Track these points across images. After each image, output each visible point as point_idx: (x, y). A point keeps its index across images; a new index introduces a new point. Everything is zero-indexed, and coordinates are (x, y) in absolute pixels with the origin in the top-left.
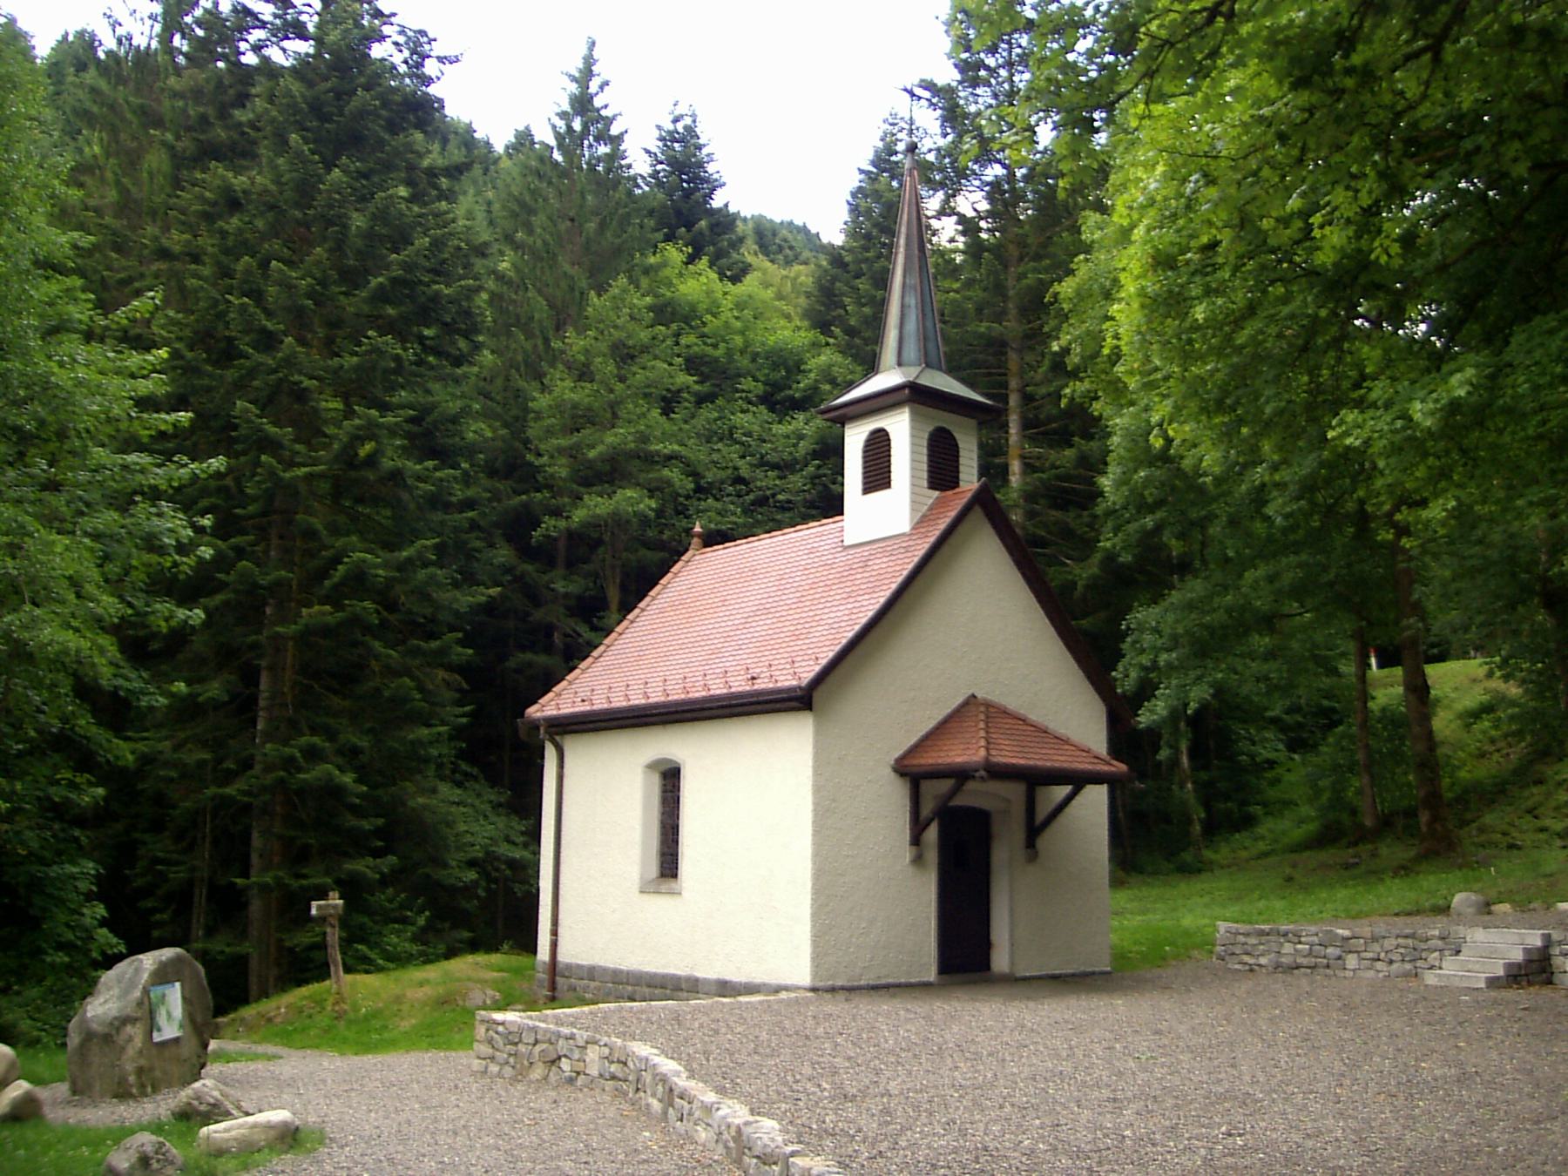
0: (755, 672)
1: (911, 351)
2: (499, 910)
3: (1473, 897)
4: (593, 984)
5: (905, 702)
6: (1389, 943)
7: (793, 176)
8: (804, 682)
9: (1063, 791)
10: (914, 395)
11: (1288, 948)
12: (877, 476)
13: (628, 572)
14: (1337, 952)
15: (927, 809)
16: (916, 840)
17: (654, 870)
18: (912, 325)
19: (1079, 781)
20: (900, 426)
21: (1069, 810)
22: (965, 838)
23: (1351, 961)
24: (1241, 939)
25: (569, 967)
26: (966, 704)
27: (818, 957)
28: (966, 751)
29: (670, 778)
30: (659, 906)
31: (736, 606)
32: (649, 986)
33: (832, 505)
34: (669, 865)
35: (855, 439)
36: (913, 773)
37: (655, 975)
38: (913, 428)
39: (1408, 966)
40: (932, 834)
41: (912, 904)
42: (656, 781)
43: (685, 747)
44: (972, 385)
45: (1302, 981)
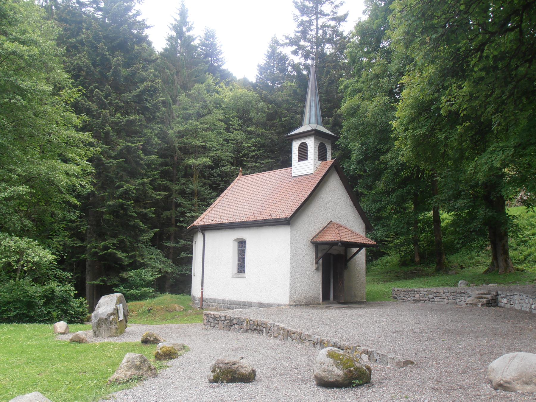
0: (271, 213)
1: (313, 119)
2: (177, 281)
3: (465, 282)
4: (215, 304)
5: (312, 224)
6: (448, 294)
7: (243, 62)
8: (289, 217)
9: (355, 250)
10: (316, 134)
11: (417, 295)
12: (303, 156)
13: (217, 182)
14: (432, 296)
15: (320, 255)
16: (317, 263)
17: (236, 270)
18: (313, 112)
19: (361, 246)
20: (311, 143)
21: (358, 255)
22: (333, 262)
23: (436, 299)
24: (403, 293)
25: (207, 299)
26: (329, 223)
27: (291, 297)
28: (331, 237)
29: (242, 244)
30: (239, 281)
31: (248, 194)
32: (235, 304)
33: (287, 163)
34: (241, 268)
35: (296, 146)
36: (317, 245)
37: (237, 301)
38: (315, 143)
39: (454, 301)
40: (321, 261)
41: (313, 282)
42: (236, 244)
43: (250, 236)
44: (332, 132)
45: (420, 304)
